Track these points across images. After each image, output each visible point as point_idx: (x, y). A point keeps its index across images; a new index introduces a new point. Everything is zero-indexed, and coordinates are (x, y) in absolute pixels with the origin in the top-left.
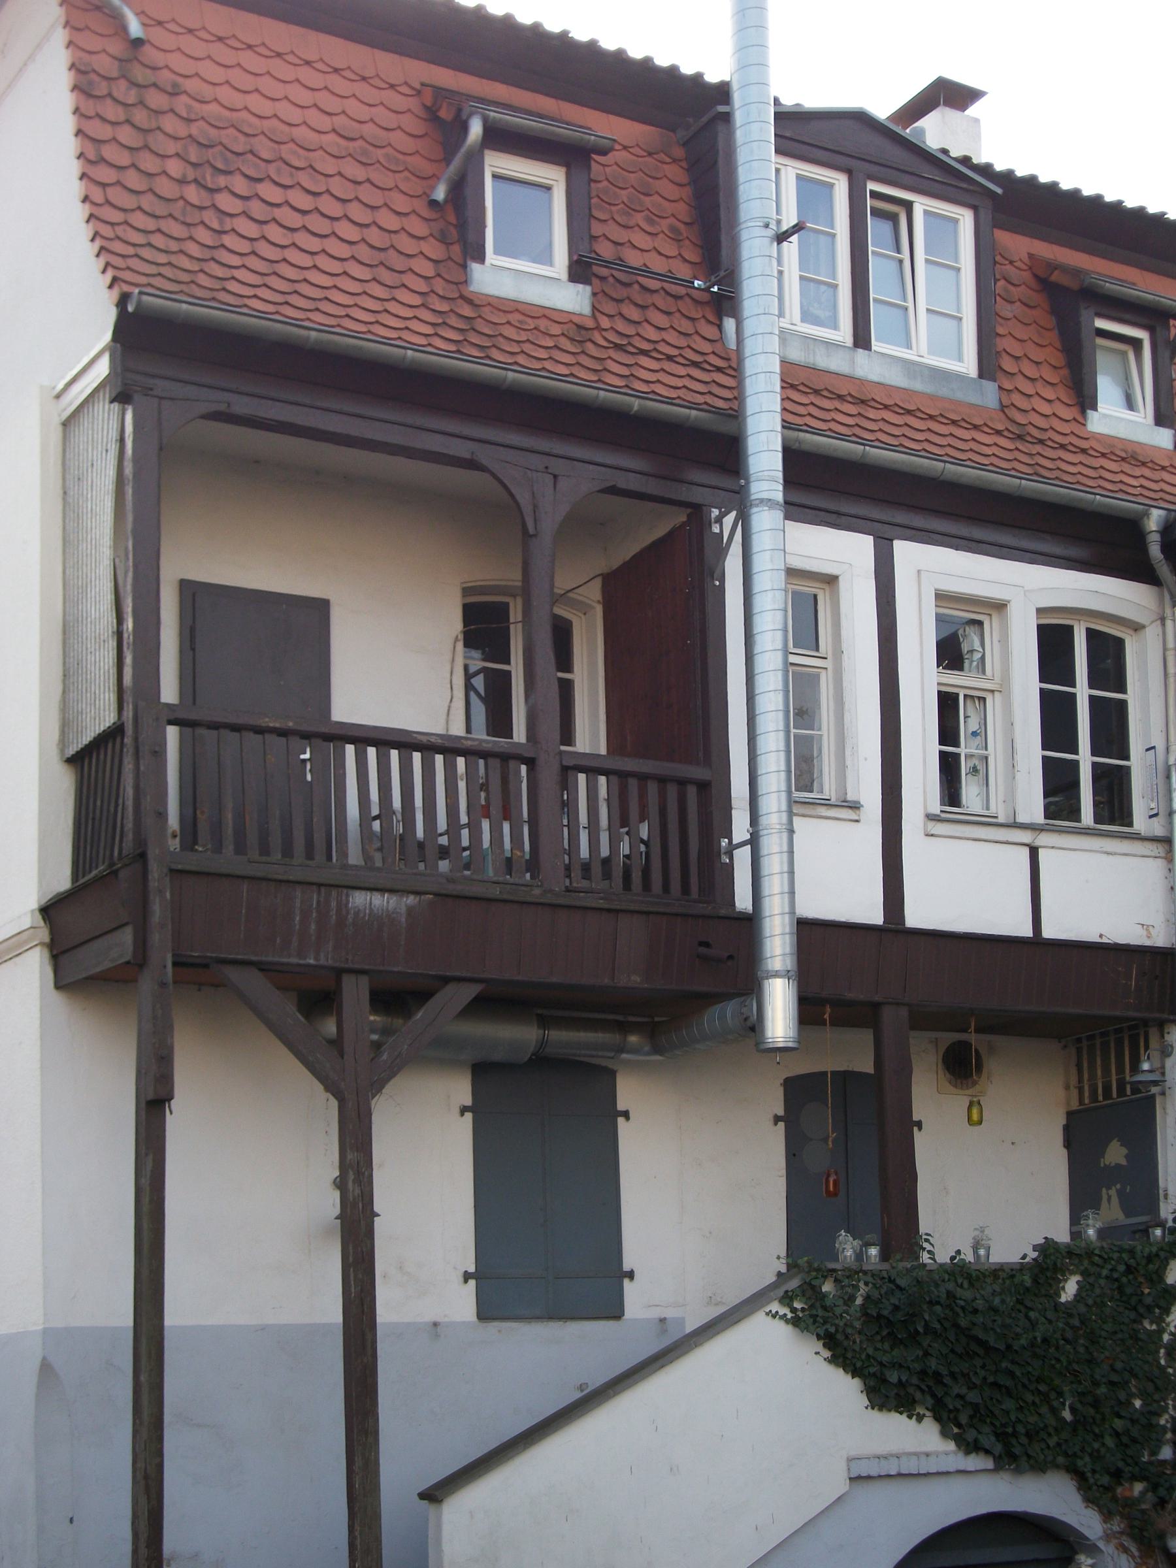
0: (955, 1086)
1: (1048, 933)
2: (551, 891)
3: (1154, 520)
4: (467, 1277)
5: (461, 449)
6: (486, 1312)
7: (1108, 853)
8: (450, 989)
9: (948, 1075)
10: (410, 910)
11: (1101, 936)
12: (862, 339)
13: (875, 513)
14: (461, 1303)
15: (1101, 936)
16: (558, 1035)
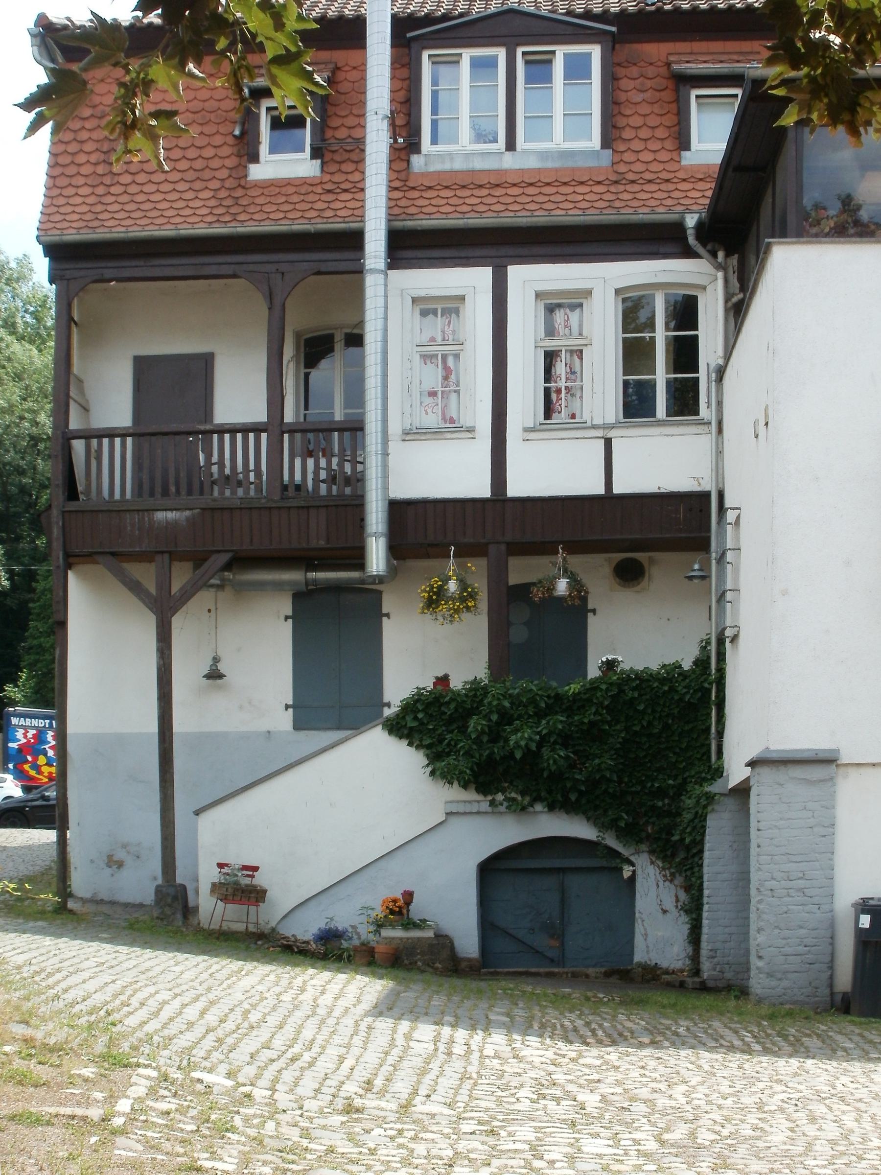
0: (624, 586)
1: (617, 489)
2: (272, 500)
3: (691, 221)
4: (287, 707)
5: (229, 270)
6: (298, 726)
7: (667, 436)
8: (214, 557)
9: (617, 579)
10: (187, 519)
11: (659, 488)
12: (511, 145)
13: (492, 251)
14: (284, 721)
15: (659, 488)
16: (312, 575)
